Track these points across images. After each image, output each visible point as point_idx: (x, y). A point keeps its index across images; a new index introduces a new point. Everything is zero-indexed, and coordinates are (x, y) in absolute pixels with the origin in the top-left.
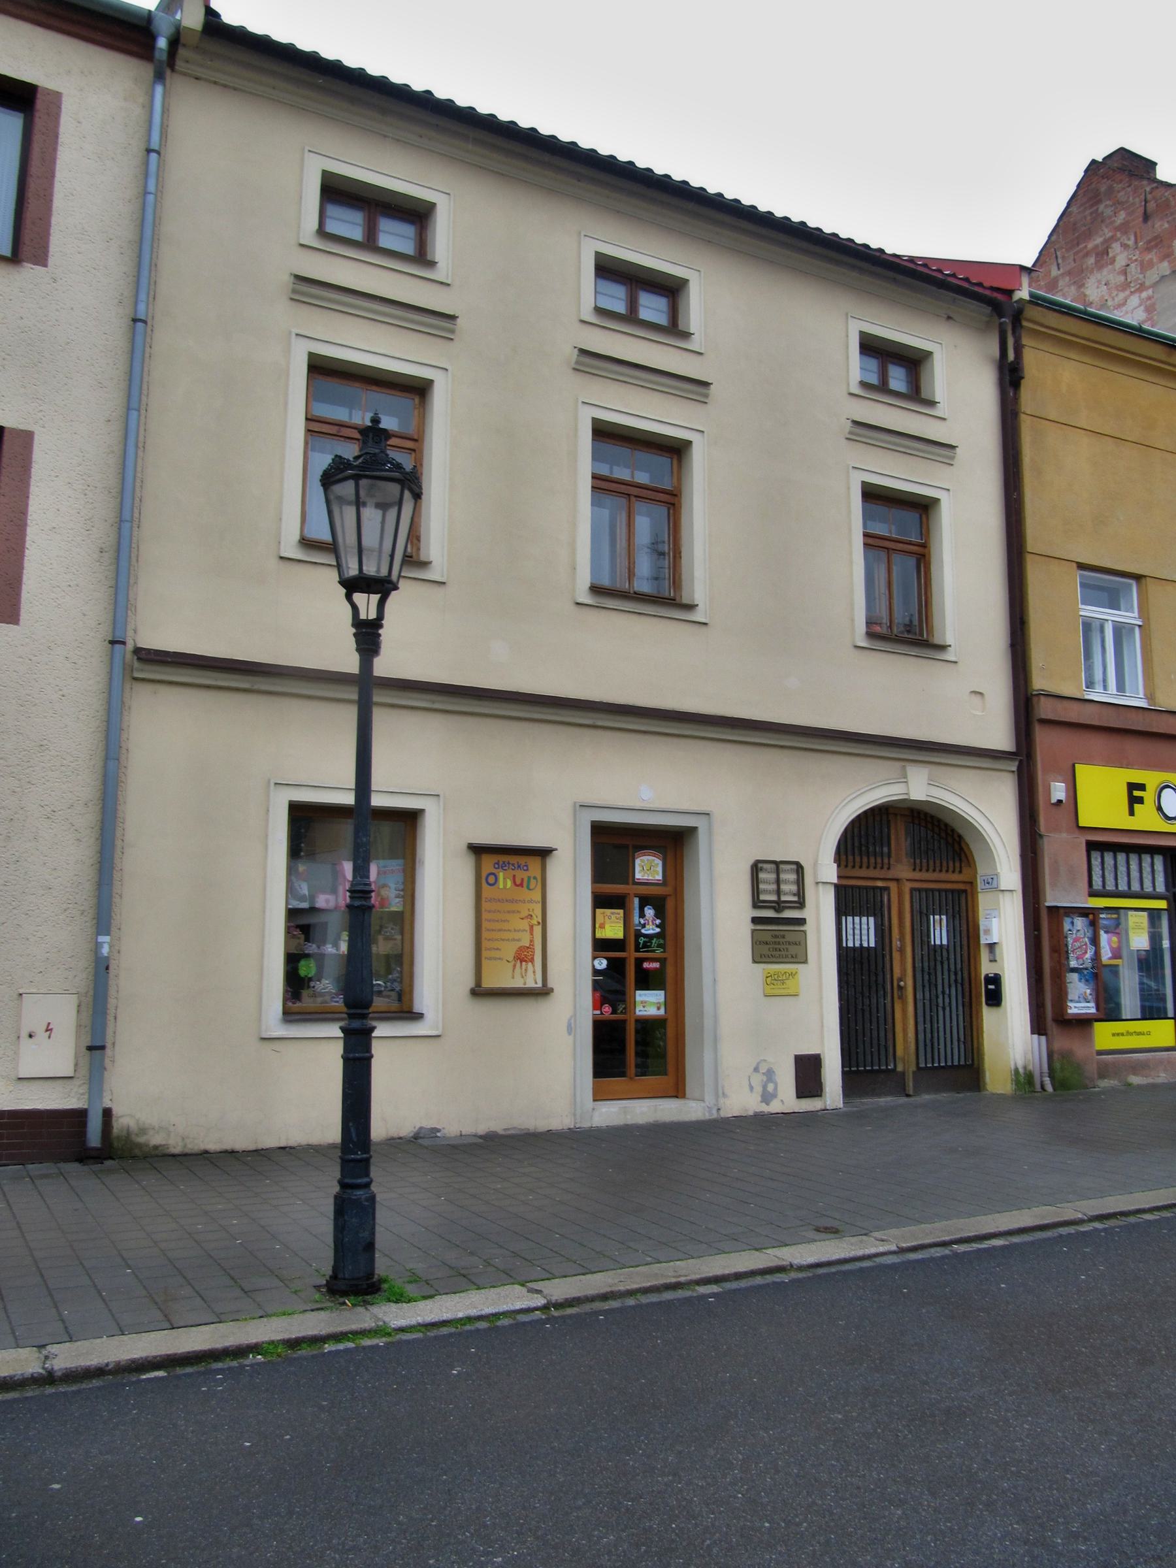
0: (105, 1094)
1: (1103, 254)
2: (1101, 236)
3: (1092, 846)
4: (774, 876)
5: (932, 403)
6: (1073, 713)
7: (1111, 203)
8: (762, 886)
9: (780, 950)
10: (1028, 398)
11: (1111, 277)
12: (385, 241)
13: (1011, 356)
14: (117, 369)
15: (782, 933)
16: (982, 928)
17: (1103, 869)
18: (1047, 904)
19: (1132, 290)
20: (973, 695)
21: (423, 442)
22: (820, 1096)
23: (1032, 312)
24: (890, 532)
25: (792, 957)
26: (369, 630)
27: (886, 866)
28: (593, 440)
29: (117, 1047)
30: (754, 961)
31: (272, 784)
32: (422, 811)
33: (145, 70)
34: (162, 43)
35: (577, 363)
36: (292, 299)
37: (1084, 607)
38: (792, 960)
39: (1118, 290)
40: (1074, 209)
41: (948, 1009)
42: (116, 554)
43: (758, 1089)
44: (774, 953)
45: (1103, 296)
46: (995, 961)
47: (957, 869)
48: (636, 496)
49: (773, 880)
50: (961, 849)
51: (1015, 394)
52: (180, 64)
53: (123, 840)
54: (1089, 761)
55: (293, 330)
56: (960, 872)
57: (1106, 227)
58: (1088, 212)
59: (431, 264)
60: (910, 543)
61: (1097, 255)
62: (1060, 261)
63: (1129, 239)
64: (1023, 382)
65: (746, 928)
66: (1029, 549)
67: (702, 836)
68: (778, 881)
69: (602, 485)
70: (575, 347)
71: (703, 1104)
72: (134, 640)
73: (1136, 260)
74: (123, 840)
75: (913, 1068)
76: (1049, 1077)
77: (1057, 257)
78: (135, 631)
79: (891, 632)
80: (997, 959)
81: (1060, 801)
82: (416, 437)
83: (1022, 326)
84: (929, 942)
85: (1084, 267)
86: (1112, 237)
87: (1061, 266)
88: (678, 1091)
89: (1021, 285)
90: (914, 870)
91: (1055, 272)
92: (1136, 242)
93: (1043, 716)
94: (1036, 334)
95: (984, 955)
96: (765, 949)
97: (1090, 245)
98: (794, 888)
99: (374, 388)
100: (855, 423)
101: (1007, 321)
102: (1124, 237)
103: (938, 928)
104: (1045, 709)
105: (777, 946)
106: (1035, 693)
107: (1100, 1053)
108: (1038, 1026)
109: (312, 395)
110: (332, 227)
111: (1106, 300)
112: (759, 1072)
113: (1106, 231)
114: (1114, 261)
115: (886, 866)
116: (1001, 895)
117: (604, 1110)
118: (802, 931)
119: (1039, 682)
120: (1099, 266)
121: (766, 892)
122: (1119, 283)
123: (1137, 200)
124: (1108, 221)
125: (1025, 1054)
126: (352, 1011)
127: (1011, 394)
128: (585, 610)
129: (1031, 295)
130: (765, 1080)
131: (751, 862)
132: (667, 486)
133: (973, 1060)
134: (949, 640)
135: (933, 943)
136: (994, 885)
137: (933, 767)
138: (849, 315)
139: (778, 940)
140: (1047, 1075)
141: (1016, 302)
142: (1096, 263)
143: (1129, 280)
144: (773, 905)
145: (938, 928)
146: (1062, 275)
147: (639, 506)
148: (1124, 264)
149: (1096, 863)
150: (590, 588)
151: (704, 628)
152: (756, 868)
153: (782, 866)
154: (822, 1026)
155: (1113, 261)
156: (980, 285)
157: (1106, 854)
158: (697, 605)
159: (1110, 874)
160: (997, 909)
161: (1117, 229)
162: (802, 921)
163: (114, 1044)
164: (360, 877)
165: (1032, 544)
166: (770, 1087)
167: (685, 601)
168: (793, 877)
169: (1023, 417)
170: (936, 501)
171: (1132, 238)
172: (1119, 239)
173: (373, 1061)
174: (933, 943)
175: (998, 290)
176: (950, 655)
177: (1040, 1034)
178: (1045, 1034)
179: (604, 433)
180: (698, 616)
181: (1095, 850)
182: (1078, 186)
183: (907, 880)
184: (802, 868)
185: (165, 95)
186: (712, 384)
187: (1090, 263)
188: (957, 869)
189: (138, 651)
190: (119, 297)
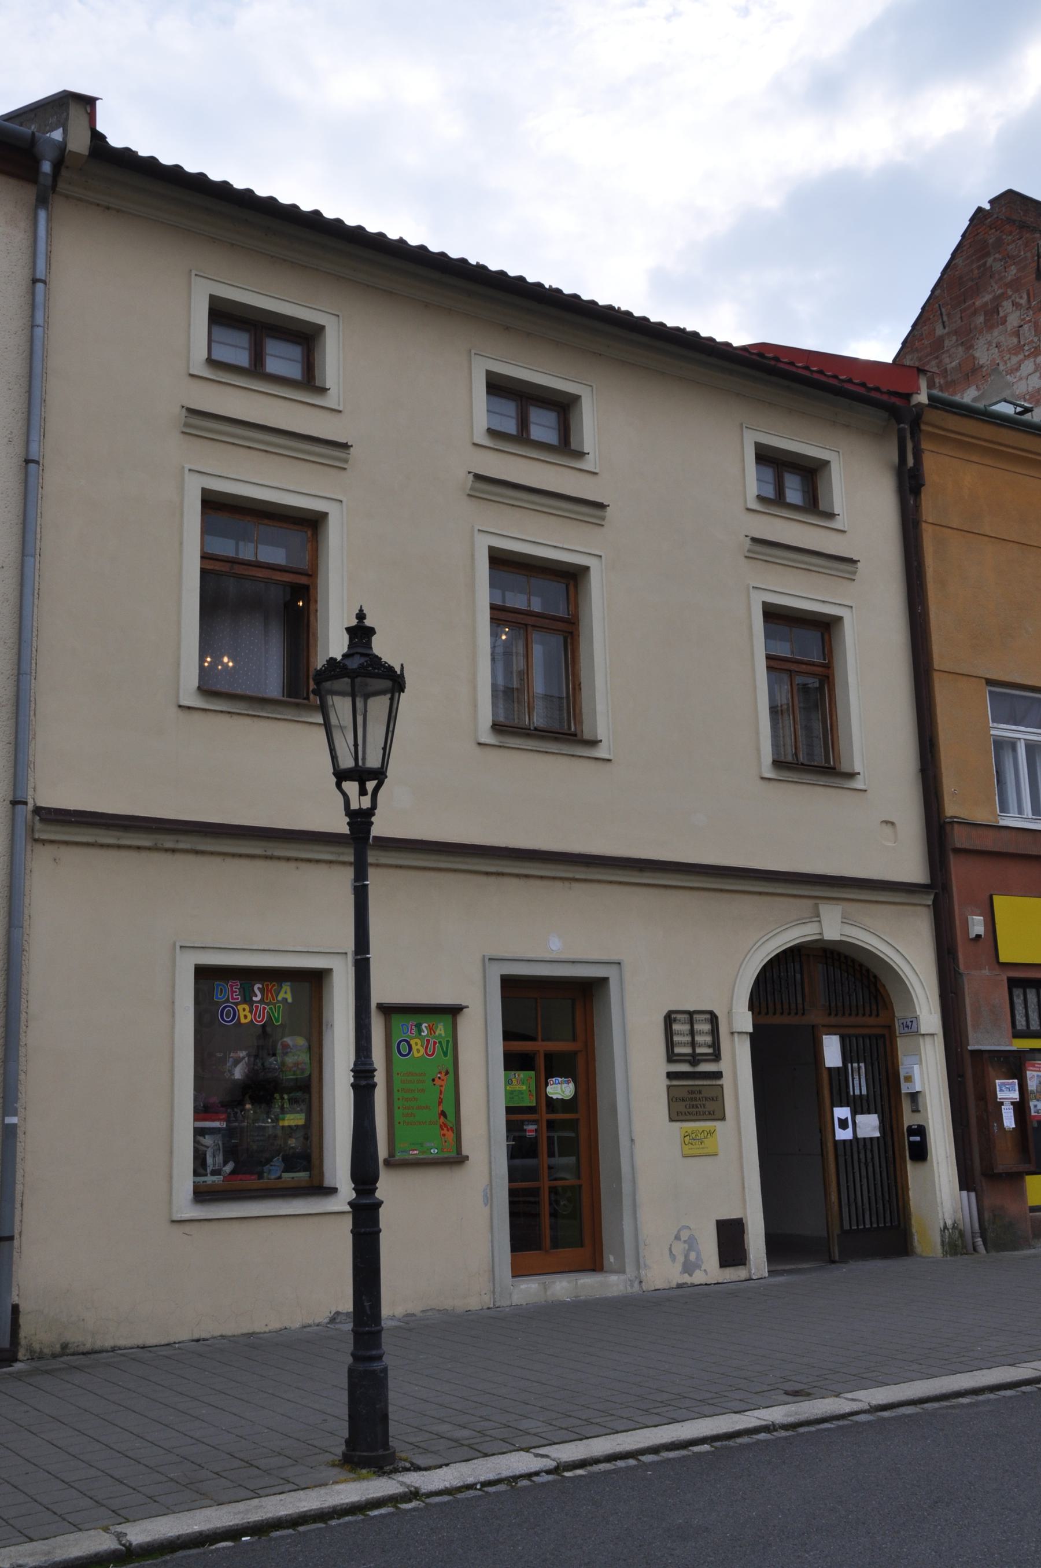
0: (13, 1289)
1: (993, 315)
2: (990, 293)
3: (1014, 983)
4: (687, 1027)
5: (831, 516)
6: (988, 842)
7: (1000, 257)
8: (676, 1039)
9: (697, 1107)
10: (929, 507)
11: (1002, 338)
12: (272, 366)
13: (910, 462)
14: (9, 512)
15: (698, 1088)
16: (902, 1074)
17: (1026, 1007)
18: (969, 1048)
19: (1027, 354)
20: (884, 825)
21: (317, 577)
22: (744, 1264)
23: (931, 416)
24: (792, 653)
25: (710, 1113)
26: (363, 820)
27: (800, 1012)
28: (490, 568)
29: (24, 1238)
30: (671, 1120)
31: (178, 948)
32: (328, 971)
33: (29, 193)
34: (46, 167)
35: (472, 489)
36: (183, 433)
37: (995, 725)
38: (710, 1117)
39: (1010, 354)
40: (959, 261)
41: (870, 1165)
42: (14, 708)
43: (681, 1259)
44: (691, 1110)
45: (994, 359)
46: (918, 1111)
47: (874, 1012)
48: (533, 626)
49: (688, 1032)
50: (877, 990)
51: (915, 500)
52: (61, 186)
53: (27, 1013)
54: (1007, 892)
55: (185, 465)
56: (878, 1015)
57: (996, 283)
58: (975, 266)
59: (323, 390)
60: (813, 664)
61: (986, 314)
62: (945, 318)
63: (1021, 298)
64: (923, 489)
65: (662, 1083)
66: (936, 667)
67: (613, 986)
68: (692, 1033)
69: (500, 615)
70: (469, 473)
71: (622, 1277)
72: (34, 799)
73: (1030, 321)
74: (27, 1013)
75: (837, 1231)
76: (981, 1237)
77: (941, 314)
78: (35, 789)
79: (797, 760)
80: (921, 1109)
81: (978, 936)
82: (310, 573)
83: (920, 430)
84: (848, 1093)
85: (972, 326)
86: (1003, 294)
87: (947, 323)
88: (595, 1265)
89: (919, 389)
90: (830, 1014)
91: (940, 331)
92: (1029, 301)
93: (958, 845)
94: (933, 436)
95: (906, 1106)
96: (681, 1106)
97: (978, 303)
98: (708, 1039)
99: (266, 521)
100: (754, 540)
101: (906, 427)
102: (1016, 295)
103: (856, 1077)
104: (960, 838)
105: (694, 1103)
106: (947, 820)
107: (1033, 1209)
108: (966, 1182)
109: (207, 529)
110: (223, 354)
111: (998, 364)
112: (680, 1239)
113: (996, 287)
114: (1006, 321)
115: (800, 1012)
116: (921, 1039)
117: (523, 1287)
118: (719, 1085)
119: (951, 809)
120: (989, 326)
121: (680, 1044)
122: (1011, 346)
123: (1029, 254)
124: (997, 276)
125: (955, 1212)
126: (361, 1187)
127: (912, 502)
128: (488, 750)
129: (930, 397)
130: (687, 1247)
131: (665, 1013)
132: (562, 613)
133: (899, 1221)
134: (857, 768)
135: (852, 1093)
136: (914, 1028)
137: (845, 904)
138: (744, 425)
139: (694, 1096)
140: (979, 1235)
141: (914, 406)
142: (985, 322)
143: (1022, 343)
144: (675, 1058)
145: (856, 1077)
146: (948, 334)
147: (535, 636)
148: (1016, 324)
149: (1018, 1001)
150: (492, 727)
151: (608, 764)
152: (669, 1019)
153: (695, 1016)
154: (744, 1188)
155: (1004, 321)
156: (877, 389)
157: (1028, 991)
158: (601, 741)
159: (1033, 1012)
160: (918, 1053)
161: (1009, 285)
162: (718, 1075)
163: (20, 1234)
164: (365, 1058)
165: (938, 663)
166: (693, 1256)
167: (587, 736)
168: (707, 1027)
169: (924, 525)
170: (839, 619)
171: (1025, 296)
172: (1010, 297)
173: (381, 1235)
174: (852, 1093)
175: (896, 394)
176: (858, 784)
177: (968, 1190)
178: (974, 1190)
179: (499, 560)
180: (601, 752)
181: (1017, 987)
182: (963, 236)
183: (823, 1026)
184: (716, 1017)
185: (49, 220)
186: (608, 506)
187: (978, 322)
188: (874, 1012)
189: (38, 810)
190: (9, 436)
